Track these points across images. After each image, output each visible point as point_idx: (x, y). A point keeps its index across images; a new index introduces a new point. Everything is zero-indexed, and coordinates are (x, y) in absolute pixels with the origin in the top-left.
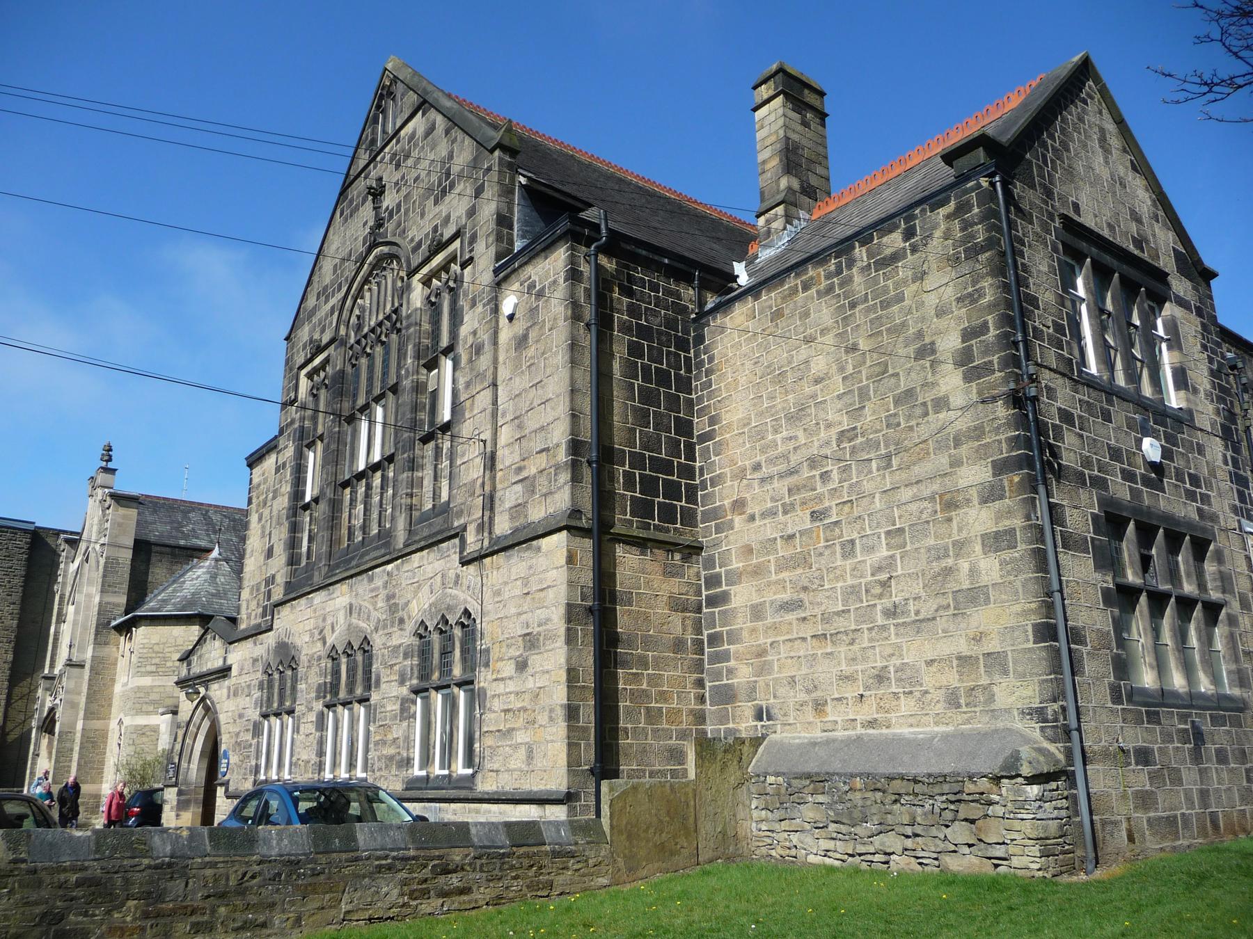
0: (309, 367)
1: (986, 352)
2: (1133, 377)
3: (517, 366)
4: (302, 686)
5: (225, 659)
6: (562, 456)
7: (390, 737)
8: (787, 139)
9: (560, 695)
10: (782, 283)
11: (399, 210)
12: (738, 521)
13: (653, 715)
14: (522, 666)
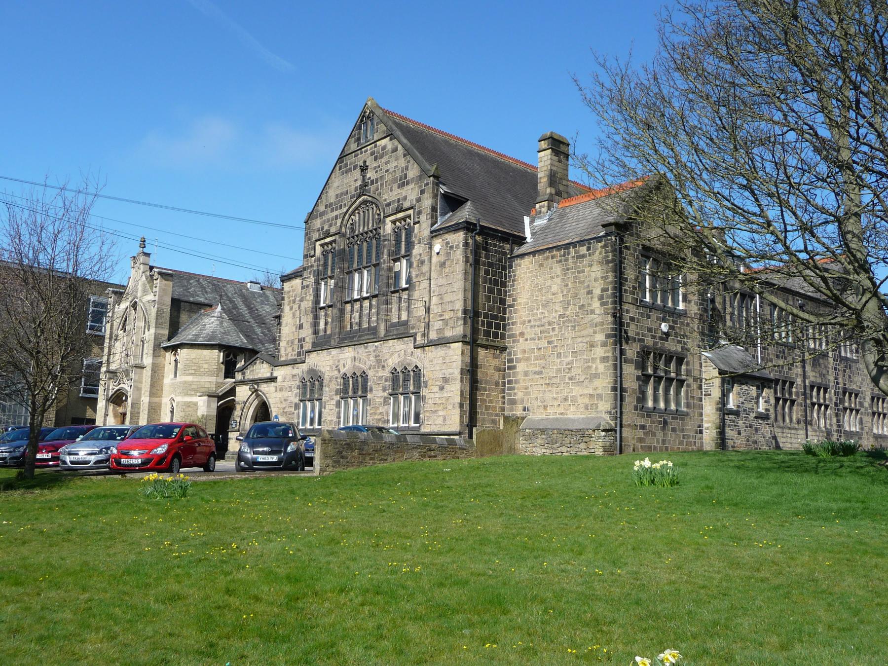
0: (322, 242)
1: (607, 298)
2: (664, 300)
3: (441, 274)
4: (326, 389)
5: (272, 373)
6: (460, 314)
7: (378, 412)
8: (551, 170)
9: (458, 399)
10: (544, 254)
11: (377, 182)
12: (521, 340)
13: (487, 408)
14: (442, 388)
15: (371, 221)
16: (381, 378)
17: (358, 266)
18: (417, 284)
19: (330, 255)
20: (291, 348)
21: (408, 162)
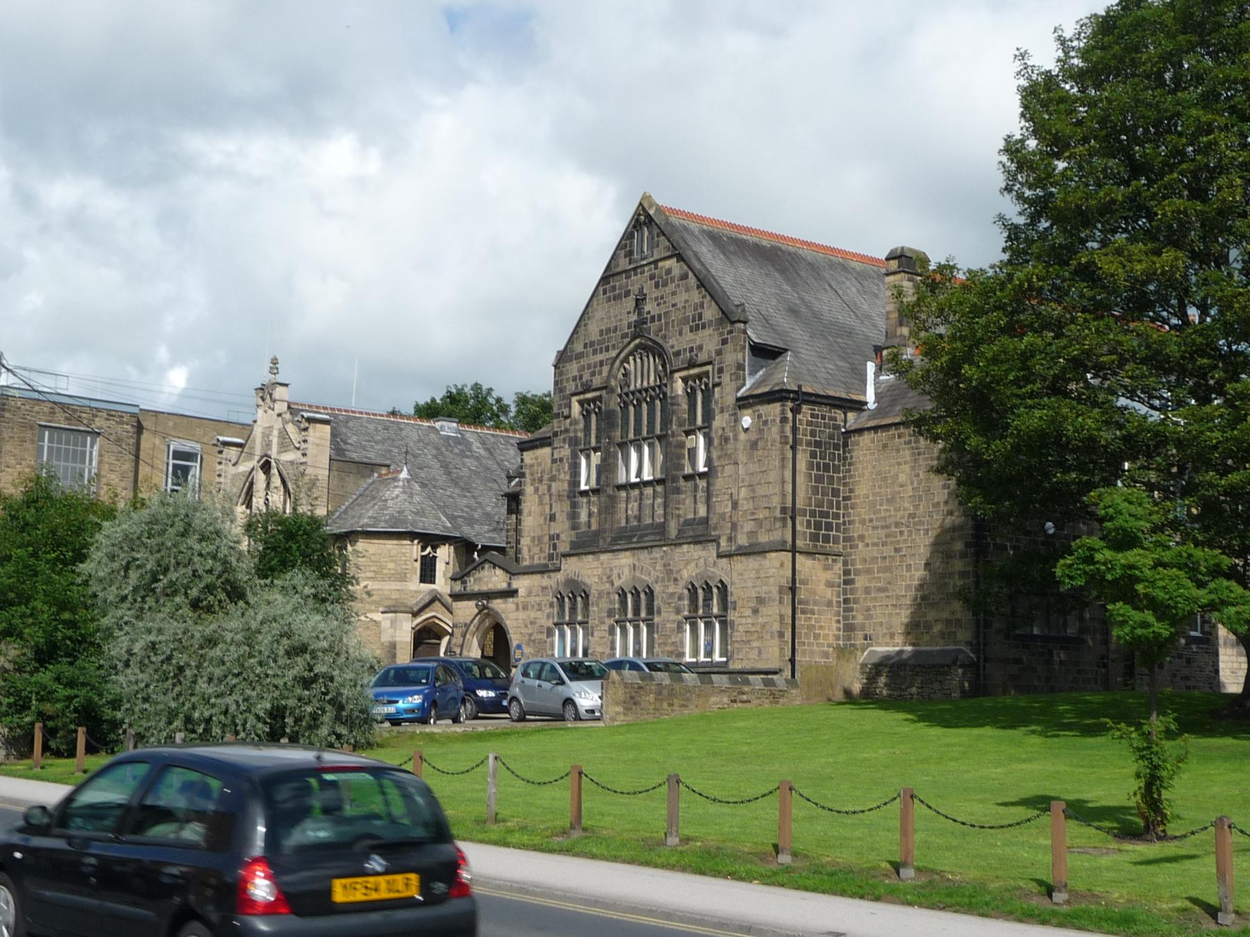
0: (582, 397)
6: (778, 514)
11: (660, 320)
12: (860, 545)
13: (817, 637)
14: (756, 611)
15: (652, 374)
16: (672, 594)
17: (635, 435)
18: (720, 469)
19: (593, 417)
20: (538, 549)
21: (704, 297)
